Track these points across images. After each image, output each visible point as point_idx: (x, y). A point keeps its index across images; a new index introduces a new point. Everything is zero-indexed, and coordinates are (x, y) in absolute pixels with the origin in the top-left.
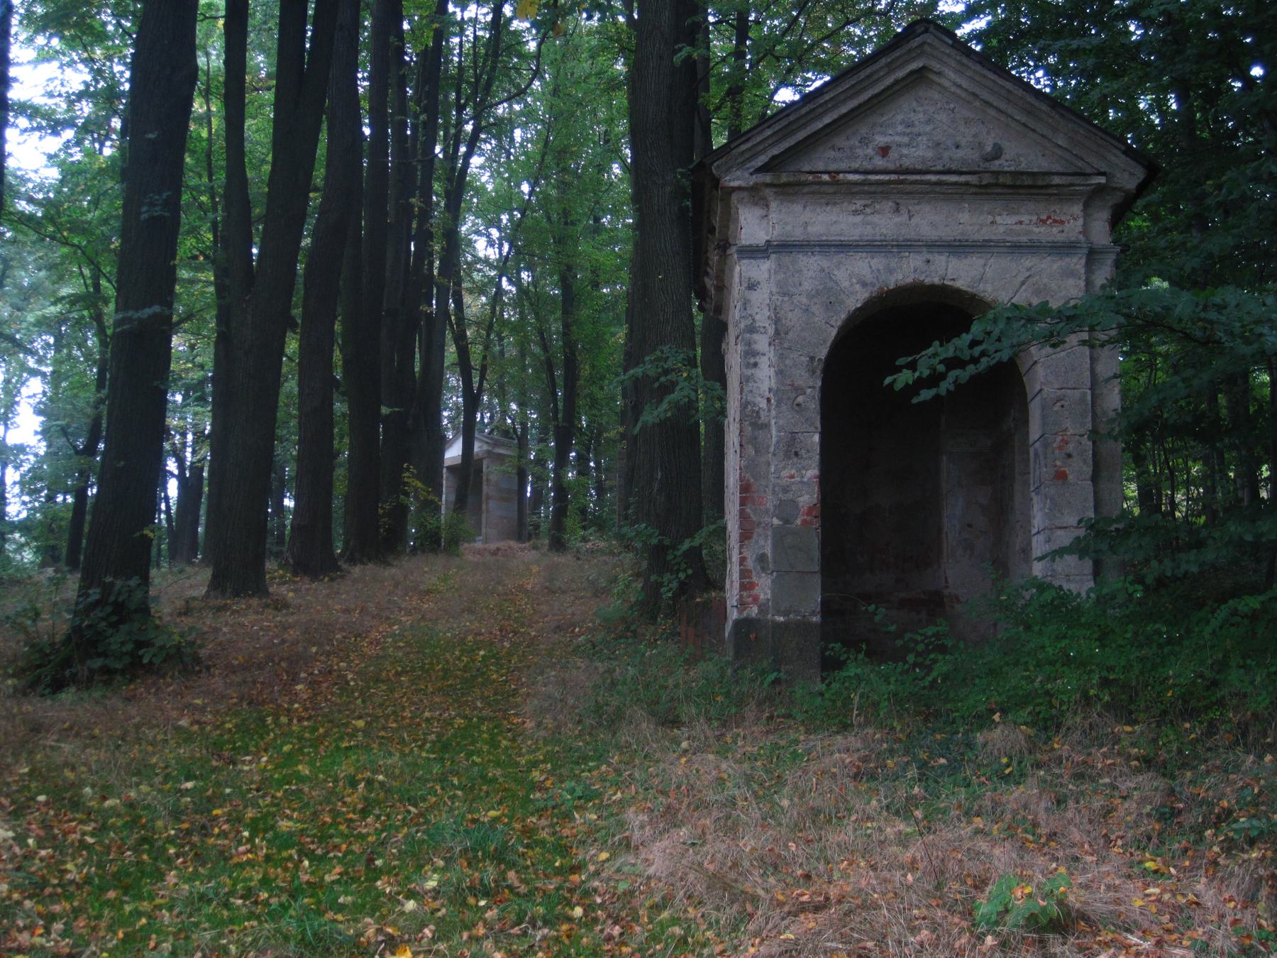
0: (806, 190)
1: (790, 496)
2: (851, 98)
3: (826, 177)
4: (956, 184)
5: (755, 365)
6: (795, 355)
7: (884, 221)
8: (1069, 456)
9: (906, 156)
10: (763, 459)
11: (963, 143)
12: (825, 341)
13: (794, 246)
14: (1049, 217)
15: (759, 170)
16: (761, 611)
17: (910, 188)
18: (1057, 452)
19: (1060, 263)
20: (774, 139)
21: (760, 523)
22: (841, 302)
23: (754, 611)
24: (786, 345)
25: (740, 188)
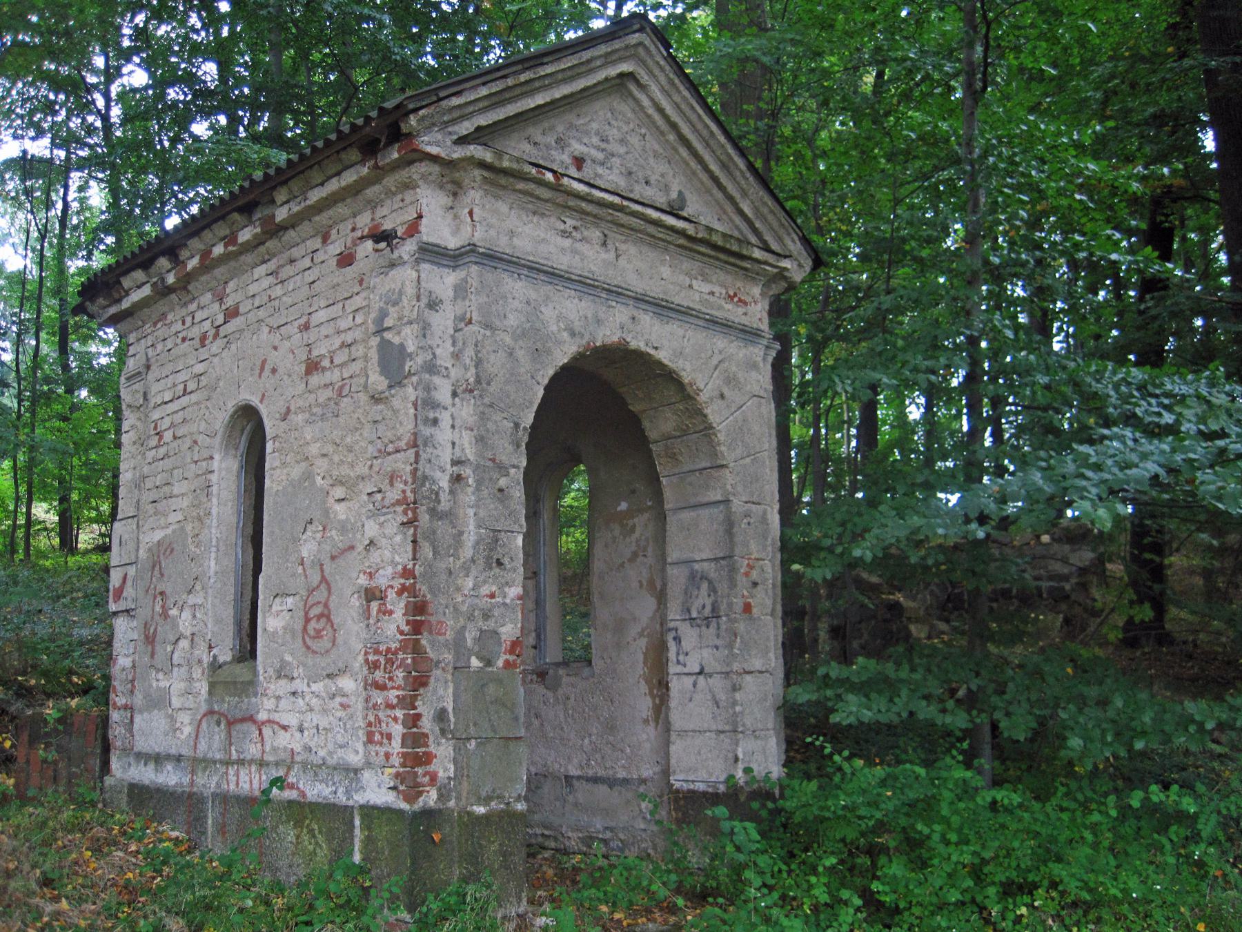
0: (521, 186)
1: (491, 624)
2: (565, 81)
3: (549, 176)
4: (672, 229)
6: (498, 417)
7: (589, 254)
8: (755, 584)
9: (600, 176)
10: (443, 565)
11: (653, 179)
12: (531, 403)
13: (501, 259)
14: (735, 295)
15: (462, 141)
16: (441, 797)
17: (634, 222)
18: (744, 579)
19: (744, 351)
20: (486, 103)
21: (439, 662)
23: (430, 798)
24: (487, 401)
25: (435, 159)
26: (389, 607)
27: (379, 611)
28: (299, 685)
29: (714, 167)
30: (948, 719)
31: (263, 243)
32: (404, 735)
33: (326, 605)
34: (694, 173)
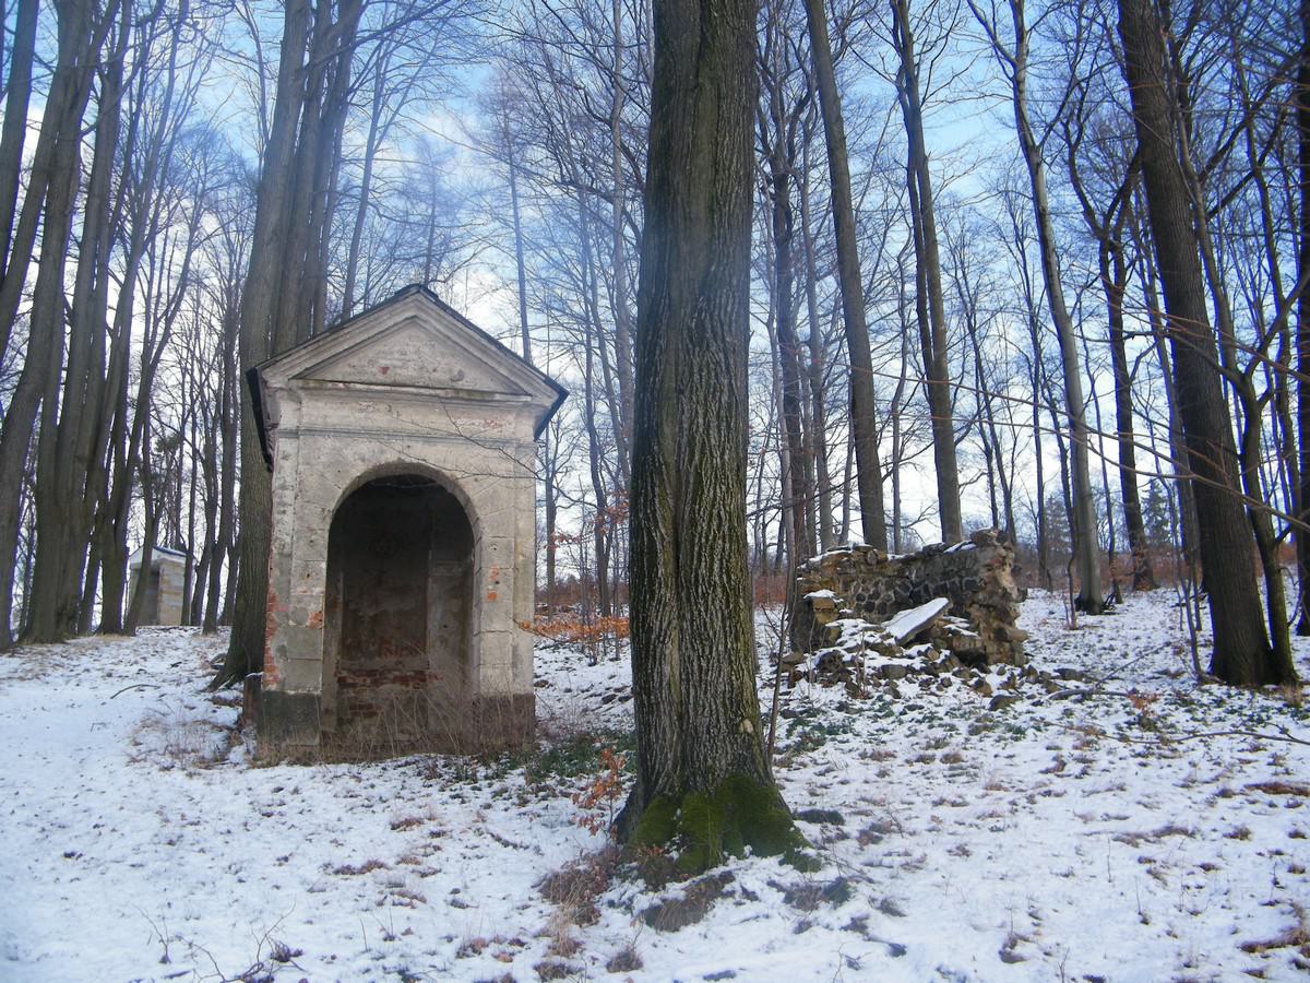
1: (302, 605)
3: (341, 385)
4: (431, 395)
5: (284, 512)
7: (380, 418)
22: (347, 471)
30: (989, 246)
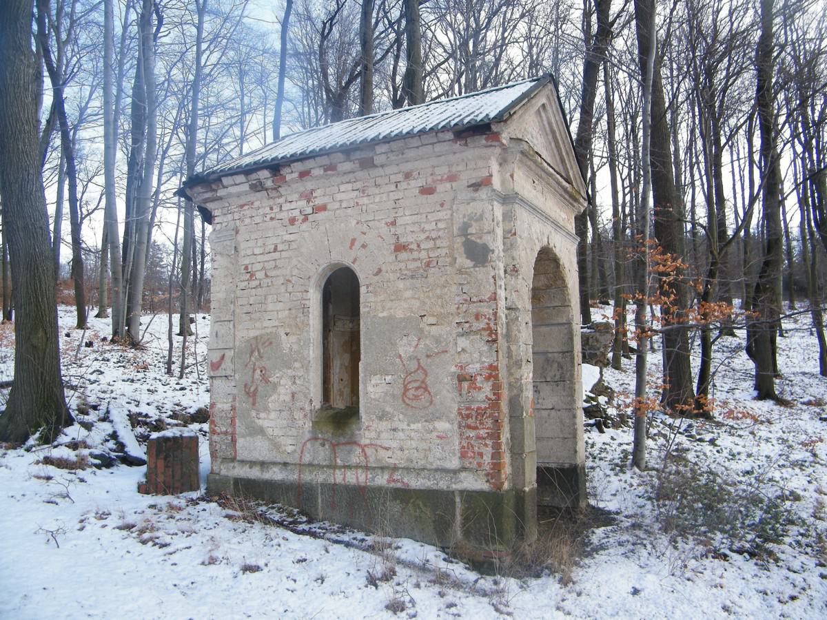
4: (563, 187)
26: (478, 385)
27: (470, 387)
28: (397, 424)
29: (564, 154)
31: (354, 172)
32: (493, 453)
33: (423, 382)
34: (555, 156)
